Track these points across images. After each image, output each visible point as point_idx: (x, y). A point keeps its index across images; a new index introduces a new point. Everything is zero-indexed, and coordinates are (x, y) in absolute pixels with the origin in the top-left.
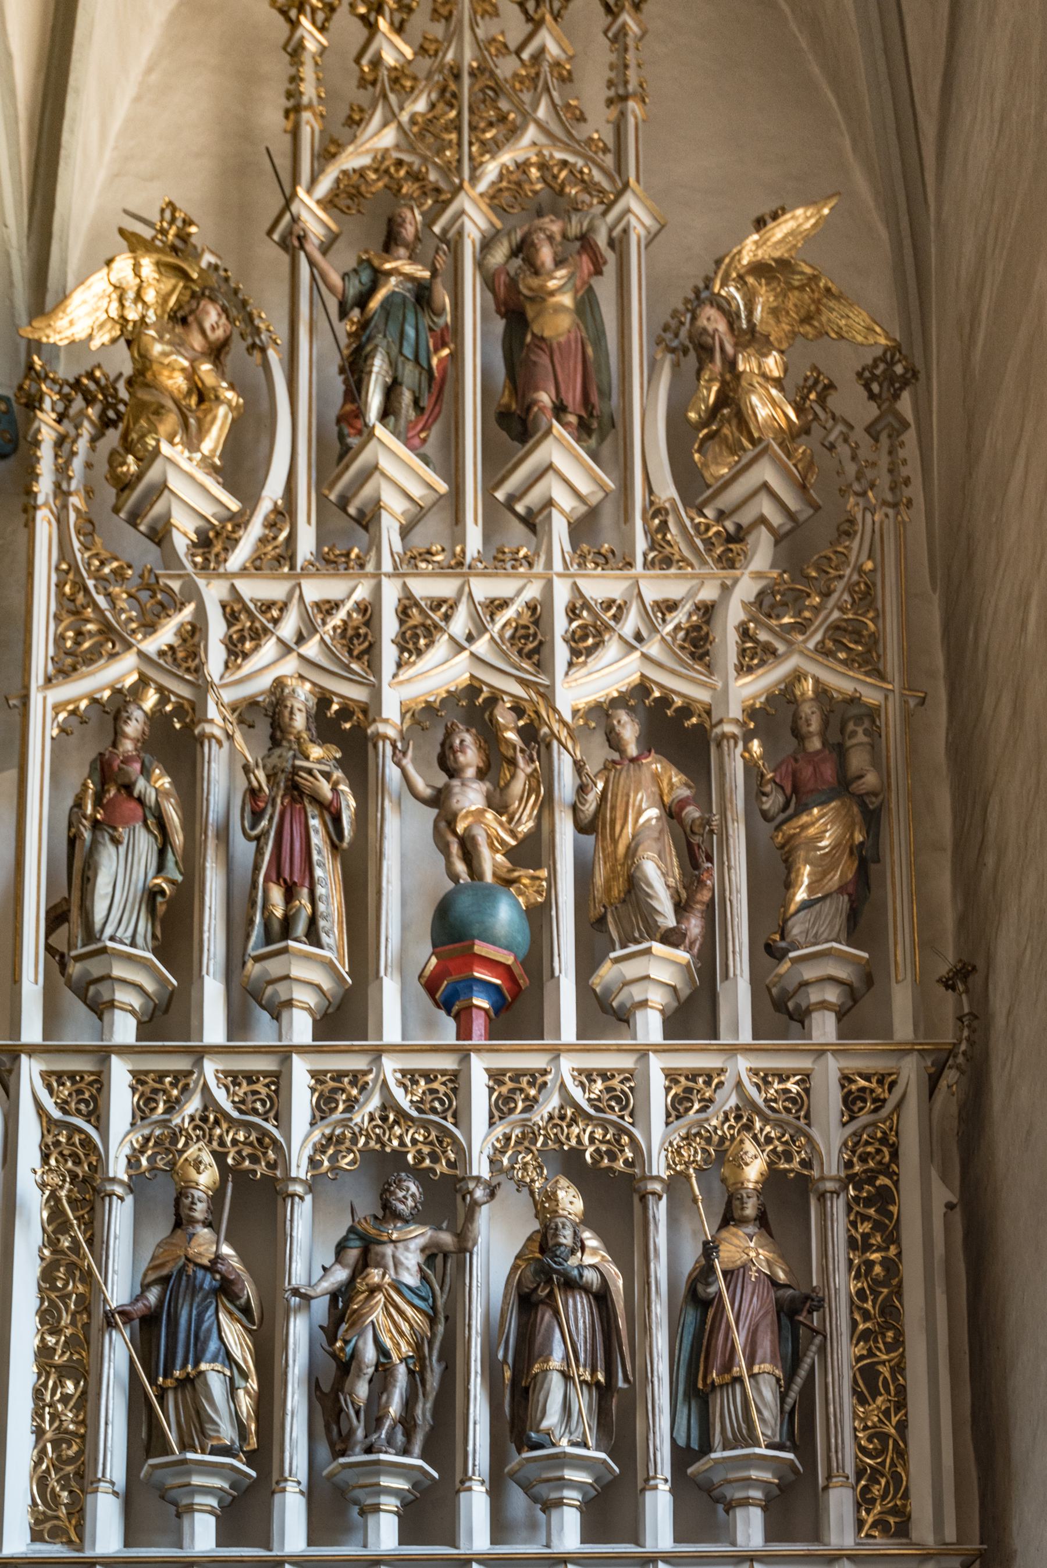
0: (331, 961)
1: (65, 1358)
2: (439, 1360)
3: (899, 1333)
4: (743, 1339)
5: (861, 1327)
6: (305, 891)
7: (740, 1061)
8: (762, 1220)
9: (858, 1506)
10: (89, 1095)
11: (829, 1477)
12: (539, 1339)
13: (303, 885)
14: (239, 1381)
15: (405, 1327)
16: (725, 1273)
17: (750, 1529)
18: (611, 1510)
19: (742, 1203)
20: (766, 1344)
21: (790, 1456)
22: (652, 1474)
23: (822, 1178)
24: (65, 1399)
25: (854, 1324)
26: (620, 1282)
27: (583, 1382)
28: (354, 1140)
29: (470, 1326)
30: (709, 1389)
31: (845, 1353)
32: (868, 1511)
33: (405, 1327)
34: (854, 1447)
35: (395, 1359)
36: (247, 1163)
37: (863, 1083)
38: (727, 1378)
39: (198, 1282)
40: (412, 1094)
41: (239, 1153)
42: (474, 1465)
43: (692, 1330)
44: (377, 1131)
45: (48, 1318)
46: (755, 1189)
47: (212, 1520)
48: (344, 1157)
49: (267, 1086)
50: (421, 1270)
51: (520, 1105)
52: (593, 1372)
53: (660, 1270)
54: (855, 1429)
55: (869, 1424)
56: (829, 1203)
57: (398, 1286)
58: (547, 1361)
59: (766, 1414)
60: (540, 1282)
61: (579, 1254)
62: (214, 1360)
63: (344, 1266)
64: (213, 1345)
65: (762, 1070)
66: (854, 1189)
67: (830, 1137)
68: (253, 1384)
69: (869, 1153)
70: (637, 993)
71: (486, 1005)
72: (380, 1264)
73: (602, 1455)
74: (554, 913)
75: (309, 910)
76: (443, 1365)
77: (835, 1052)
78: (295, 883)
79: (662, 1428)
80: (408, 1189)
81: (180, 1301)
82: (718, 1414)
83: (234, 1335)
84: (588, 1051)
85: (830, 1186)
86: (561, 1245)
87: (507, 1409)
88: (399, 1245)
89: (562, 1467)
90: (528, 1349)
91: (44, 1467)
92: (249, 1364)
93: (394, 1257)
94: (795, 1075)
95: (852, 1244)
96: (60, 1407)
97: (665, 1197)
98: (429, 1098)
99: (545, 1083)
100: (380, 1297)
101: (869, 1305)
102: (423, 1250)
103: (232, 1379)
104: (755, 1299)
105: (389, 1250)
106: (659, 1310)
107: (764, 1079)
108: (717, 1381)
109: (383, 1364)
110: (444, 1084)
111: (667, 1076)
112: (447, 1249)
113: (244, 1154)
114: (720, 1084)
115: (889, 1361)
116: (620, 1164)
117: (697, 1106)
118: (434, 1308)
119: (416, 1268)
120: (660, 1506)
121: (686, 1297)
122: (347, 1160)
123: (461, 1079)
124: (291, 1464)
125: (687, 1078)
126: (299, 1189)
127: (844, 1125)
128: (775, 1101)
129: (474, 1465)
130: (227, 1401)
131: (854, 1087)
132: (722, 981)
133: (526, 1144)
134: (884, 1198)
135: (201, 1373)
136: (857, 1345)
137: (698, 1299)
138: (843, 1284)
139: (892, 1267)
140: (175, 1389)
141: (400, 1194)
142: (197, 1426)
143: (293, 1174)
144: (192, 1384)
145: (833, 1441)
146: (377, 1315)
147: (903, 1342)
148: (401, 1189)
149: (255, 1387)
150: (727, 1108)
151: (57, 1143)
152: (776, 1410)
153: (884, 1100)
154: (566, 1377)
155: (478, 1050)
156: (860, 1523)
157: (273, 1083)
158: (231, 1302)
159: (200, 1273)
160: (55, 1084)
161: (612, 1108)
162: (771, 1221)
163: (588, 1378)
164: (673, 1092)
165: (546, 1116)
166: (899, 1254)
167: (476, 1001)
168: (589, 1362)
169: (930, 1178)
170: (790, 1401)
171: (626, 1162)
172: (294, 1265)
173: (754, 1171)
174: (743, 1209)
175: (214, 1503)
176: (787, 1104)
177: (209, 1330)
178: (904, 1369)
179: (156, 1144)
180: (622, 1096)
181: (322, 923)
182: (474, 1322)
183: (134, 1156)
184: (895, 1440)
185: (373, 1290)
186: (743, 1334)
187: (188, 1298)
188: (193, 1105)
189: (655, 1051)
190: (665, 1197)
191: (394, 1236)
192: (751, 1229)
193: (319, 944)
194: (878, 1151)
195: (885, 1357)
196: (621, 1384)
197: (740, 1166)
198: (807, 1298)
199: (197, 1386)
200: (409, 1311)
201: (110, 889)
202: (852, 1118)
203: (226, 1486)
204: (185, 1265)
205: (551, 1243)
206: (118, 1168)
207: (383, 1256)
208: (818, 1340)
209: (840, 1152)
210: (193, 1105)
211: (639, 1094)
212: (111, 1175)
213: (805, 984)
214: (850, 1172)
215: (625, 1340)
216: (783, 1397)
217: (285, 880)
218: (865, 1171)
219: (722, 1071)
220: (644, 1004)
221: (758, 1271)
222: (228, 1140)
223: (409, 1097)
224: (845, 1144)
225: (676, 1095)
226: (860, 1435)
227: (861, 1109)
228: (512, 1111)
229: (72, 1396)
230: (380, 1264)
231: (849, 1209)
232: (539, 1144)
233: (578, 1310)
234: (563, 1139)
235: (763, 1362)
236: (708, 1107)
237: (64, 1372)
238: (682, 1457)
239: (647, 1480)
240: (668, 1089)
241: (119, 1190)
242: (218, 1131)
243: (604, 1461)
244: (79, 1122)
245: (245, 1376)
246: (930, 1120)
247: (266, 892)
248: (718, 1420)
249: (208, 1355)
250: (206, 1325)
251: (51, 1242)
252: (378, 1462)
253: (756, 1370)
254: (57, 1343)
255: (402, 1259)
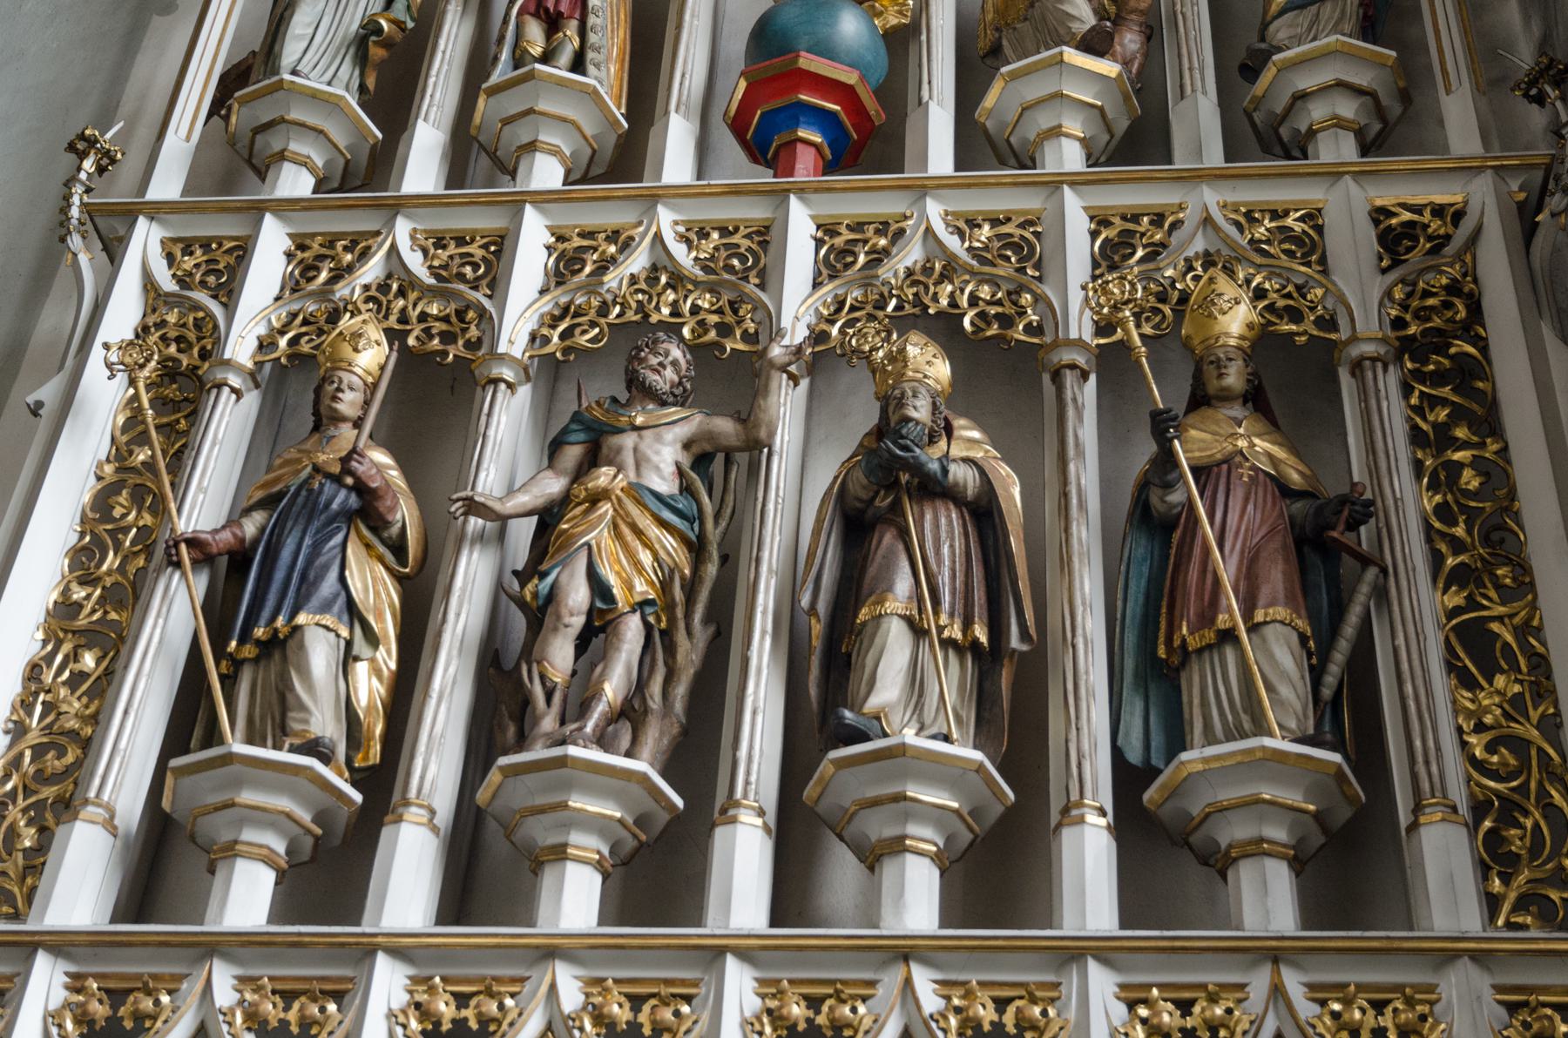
0: (596, 92)
1: (95, 617)
2: (707, 620)
3: (1523, 569)
4: (1233, 568)
5: (1450, 562)
6: (574, 23)
7: (1204, 193)
8: (1256, 398)
9: (1484, 870)
10: (225, 270)
11: (1418, 809)
12: (872, 571)
13: (571, 17)
14: (360, 646)
15: (646, 558)
16: (1196, 471)
17: (1269, 900)
18: (998, 870)
19: (1219, 367)
20: (1275, 577)
21: (1336, 757)
22: (1074, 796)
23: (1354, 339)
24: (78, 678)
25: (1436, 560)
26: (1016, 492)
27: (948, 643)
28: (604, 310)
29: (758, 560)
30: (1176, 660)
31: (1426, 605)
32: (1506, 879)
33: (646, 558)
34: (1460, 759)
35: (622, 602)
36: (436, 341)
37: (1407, 216)
38: (1210, 636)
39: (323, 499)
40: (698, 249)
41: (427, 331)
42: (747, 783)
43: (1145, 570)
44: (640, 296)
45: (83, 561)
46: (1238, 348)
47: (268, 877)
48: (584, 332)
49: (485, 247)
50: (680, 472)
51: (862, 259)
52: (967, 625)
53: (1086, 475)
54: (1460, 730)
55: (1488, 719)
56: (1370, 374)
57: (637, 492)
58: (881, 602)
59: (1285, 691)
60: (880, 494)
61: (943, 444)
62: (325, 608)
63: (558, 473)
64: (329, 584)
65: (1244, 204)
66: (1412, 360)
67: (1360, 293)
68: (388, 658)
69: (1432, 308)
70: (1043, 120)
71: (817, 139)
72: (614, 461)
73: (978, 755)
74: (924, 37)
75: (576, 42)
76: (712, 629)
77: (1357, 175)
78: (560, 14)
79: (1090, 726)
80: (667, 354)
81: (289, 524)
82: (1196, 701)
83: (371, 583)
84: (969, 186)
85: (1369, 349)
86: (908, 420)
87: (813, 691)
88: (645, 433)
89: (905, 775)
90: (855, 587)
91: (9, 786)
92: (388, 627)
93: (635, 450)
94: (1297, 210)
95: (1417, 437)
96: (63, 692)
97: (1093, 378)
98: (723, 254)
99: (902, 232)
100: (606, 508)
101: (1460, 531)
102: (687, 446)
103: (349, 644)
104: (1250, 507)
105: (629, 440)
106: (1086, 536)
107: (1249, 215)
108: (1193, 643)
109: (601, 611)
110: (746, 236)
111: (1092, 218)
112: (725, 443)
113: (434, 331)
114: (1175, 225)
115: (1511, 616)
116: (1018, 333)
117: (1140, 253)
118: (702, 537)
119: (673, 469)
120: (1089, 859)
121: (1131, 514)
122: (588, 337)
123: (774, 232)
124: (422, 778)
125: (1124, 218)
126: (508, 374)
127: (1384, 271)
128: (1268, 242)
129: (747, 783)
130: (338, 677)
131: (1394, 221)
132: (1176, 104)
133: (869, 309)
134: (1471, 376)
135: (297, 629)
136: (1445, 592)
137: (1153, 528)
138: (1409, 500)
139: (1497, 474)
140: (256, 661)
141: (654, 361)
142: (276, 717)
143: (501, 349)
144: (281, 649)
145: (1418, 743)
146: (599, 535)
147: (1532, 584)
148: (657, 354)
149: (393, 666)
150: (1190, 253)
151: (162, 324)
152: (1304, 687)
153: (1448, 237)
154: (918, 631)
155: (802, 191)
156: (1492, 903)
157: (494, 243)
158: (375, 530)
159: (329, 487)
160: (179, 254)
161: (1008, 259)
162: (1277, 413)
163: (957, 634)
164: (1103, 236)
165: (902, 274)
166: (1504, 451)
167: (802, 133)
168: (959, 607)
169: (1542, 340)
170: (1330, 680)
171: (1029, 329)
172: (482, 475)
173: (1236, 320)
174: (1221, 376)
175: (280, 847)
176: (1286, 246)
177: (326, 568)
178: (1540, 629)
179: (305, 322)
180: (1024, 250)
181: (590, 55)
182: (766, 555)
183: (269, 336)
184: (1540, 750)
185: (595, 499)
186: (1234, 561)
187: (302, 521)
188: (372, 271)
189: (1072, 184)
190: (1093, 378)
191: (639, 420)
192: (1237, 411)
193: (584, 73)
194: (1447, 305)
195: (1501, 610)
196: (1015, 642)
197: (1211, 315)
198: (1343, 500)
199: (289, 652)
200: (654, 531)
201: (311, 31)
202: (1396, 263)
203: (306, 817)
204: (311, 477)
205: (894, 419)
206: (241, 346)
207: (619, 450)
208: (1371, 573)
209: (1381, 304)
210: (372, 271)
211: (1049, 241)
212: (227, 356)
213: (1301, 97)
214: (1403, 333)
215: (1024, 585)
216: (1316, 675)
217: (547, 10)
218: (1425, 332)
219: (1181, 208)
220: (1056, 132)
221: (1254, 468)
222: (414, 314)
223: (694, 254)
224: (1388, 294)
225: (1106, 240)
226: (1473, 740)
227: (1409, 250)
228: (847, 266)
229: (88, 675)
230: (614, 461)
231: (1407, 390)
232: (890, 308)
233: (942, 535)
234: (927, 301)
235: (1271, 604)
236: (1159, 254)
237: (88, 637)
238: (1130, 779)
239: (1066, 811)
240: (1094, 235)
241: (235, 380)
242: (401, 303)
243: (980, 768)
244: (201, 297)
245: (373, 640)
246: (1530, 269)
247: (519, 27)
248: (1197, 711)
249: (315, 601)
250: (322, 560)
251: (120, 454)
252: (563, 761)
253: (1259, 616)
254: (88, 597)
255: (649, 453)
